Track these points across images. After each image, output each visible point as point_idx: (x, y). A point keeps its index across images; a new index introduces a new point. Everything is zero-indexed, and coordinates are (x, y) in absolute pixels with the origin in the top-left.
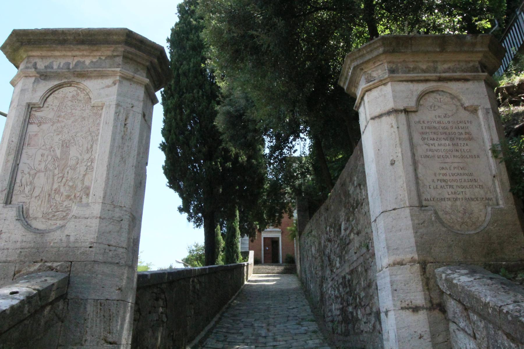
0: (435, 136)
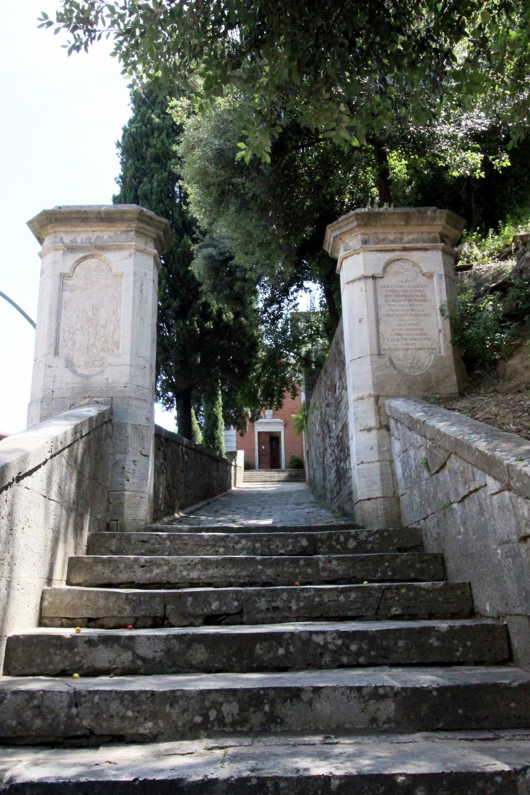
0: (397, 298)
